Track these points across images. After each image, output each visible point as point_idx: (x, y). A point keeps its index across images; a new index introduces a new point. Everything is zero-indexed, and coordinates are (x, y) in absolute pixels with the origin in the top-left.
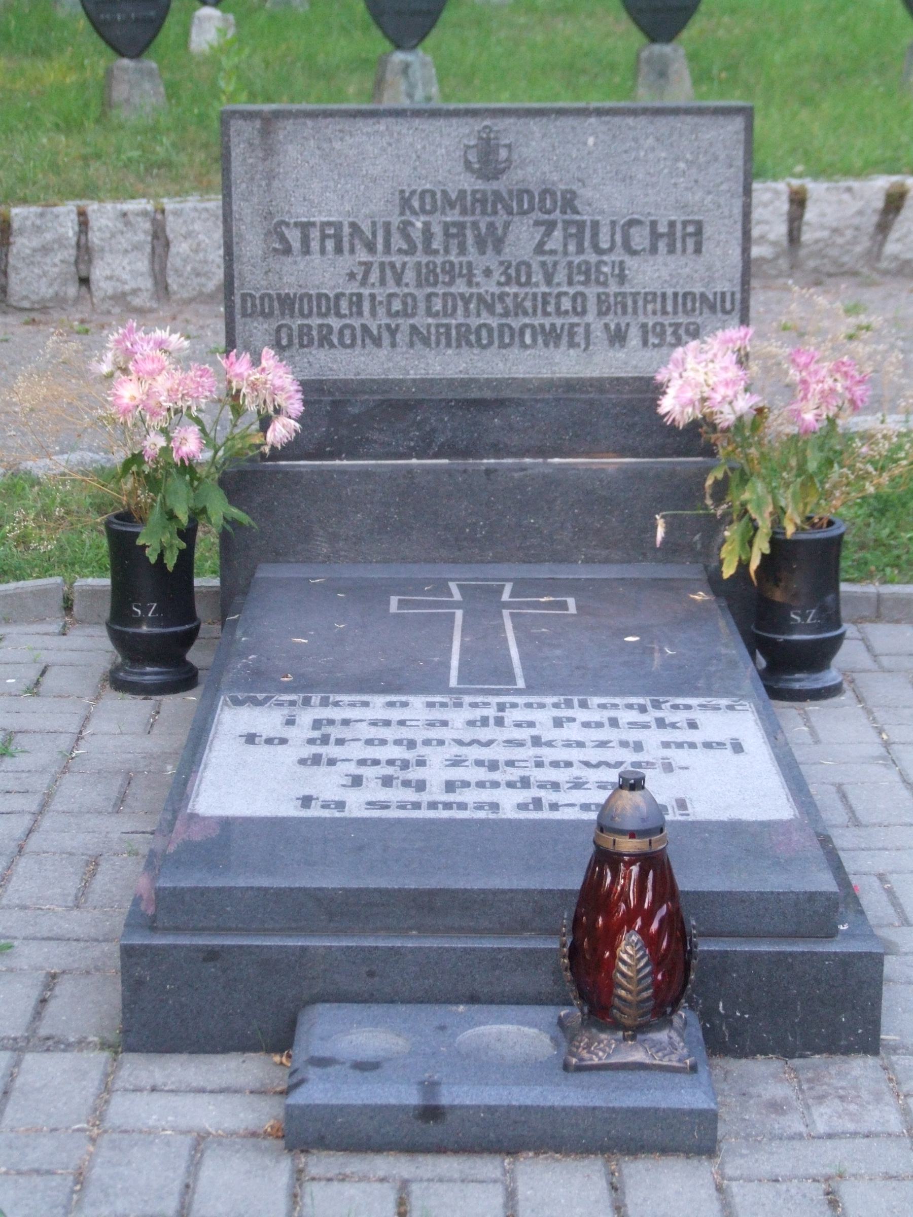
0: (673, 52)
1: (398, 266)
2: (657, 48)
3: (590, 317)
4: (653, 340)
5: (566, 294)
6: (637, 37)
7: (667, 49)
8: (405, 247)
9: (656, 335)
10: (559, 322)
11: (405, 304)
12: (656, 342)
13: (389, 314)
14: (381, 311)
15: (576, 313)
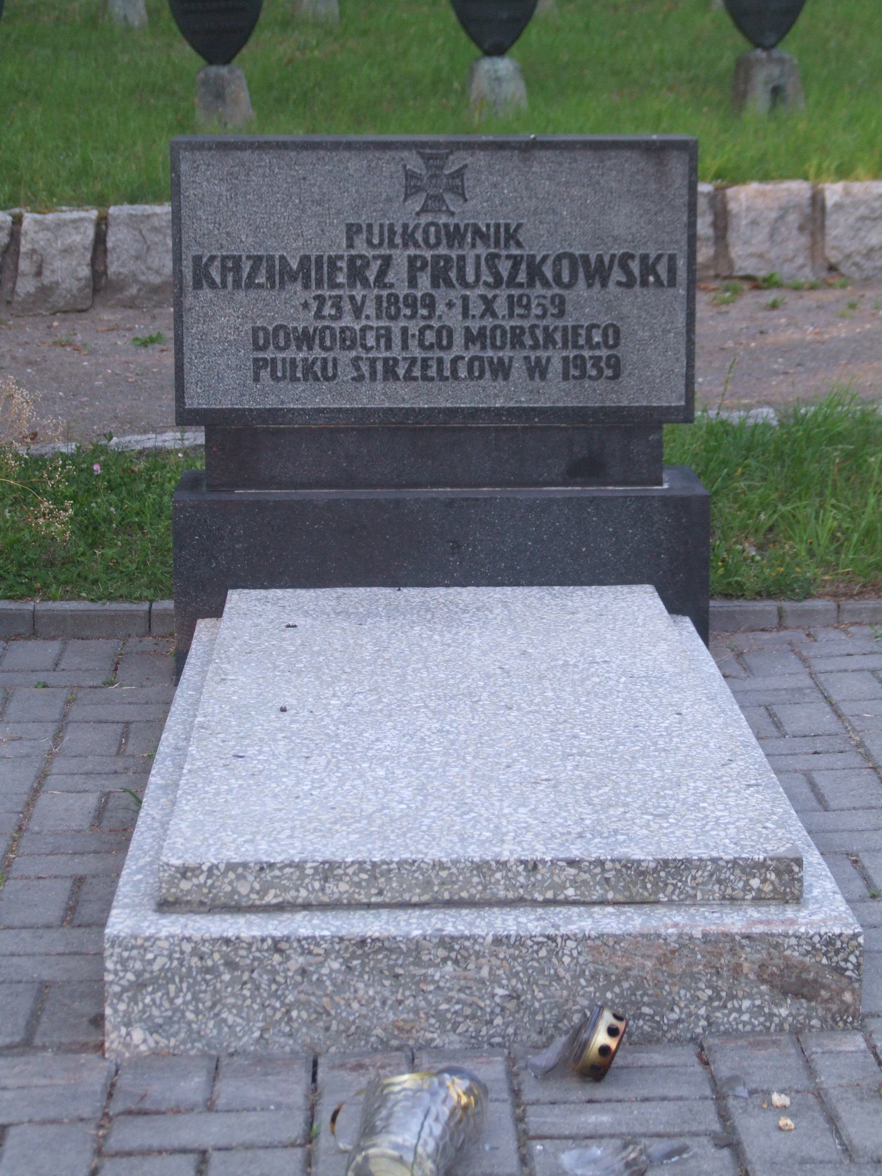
0: (237, 76)
1: (359, 299)
2: (214, 70)
3: (456, 351)
4: (574, 372)
6: (200, 61)
7: (224, 71)
8: (624, 279)
10: (587, 353)
11: (605, 335)
13: (421, 345)
14: (413, 344)
15: (441, 348)
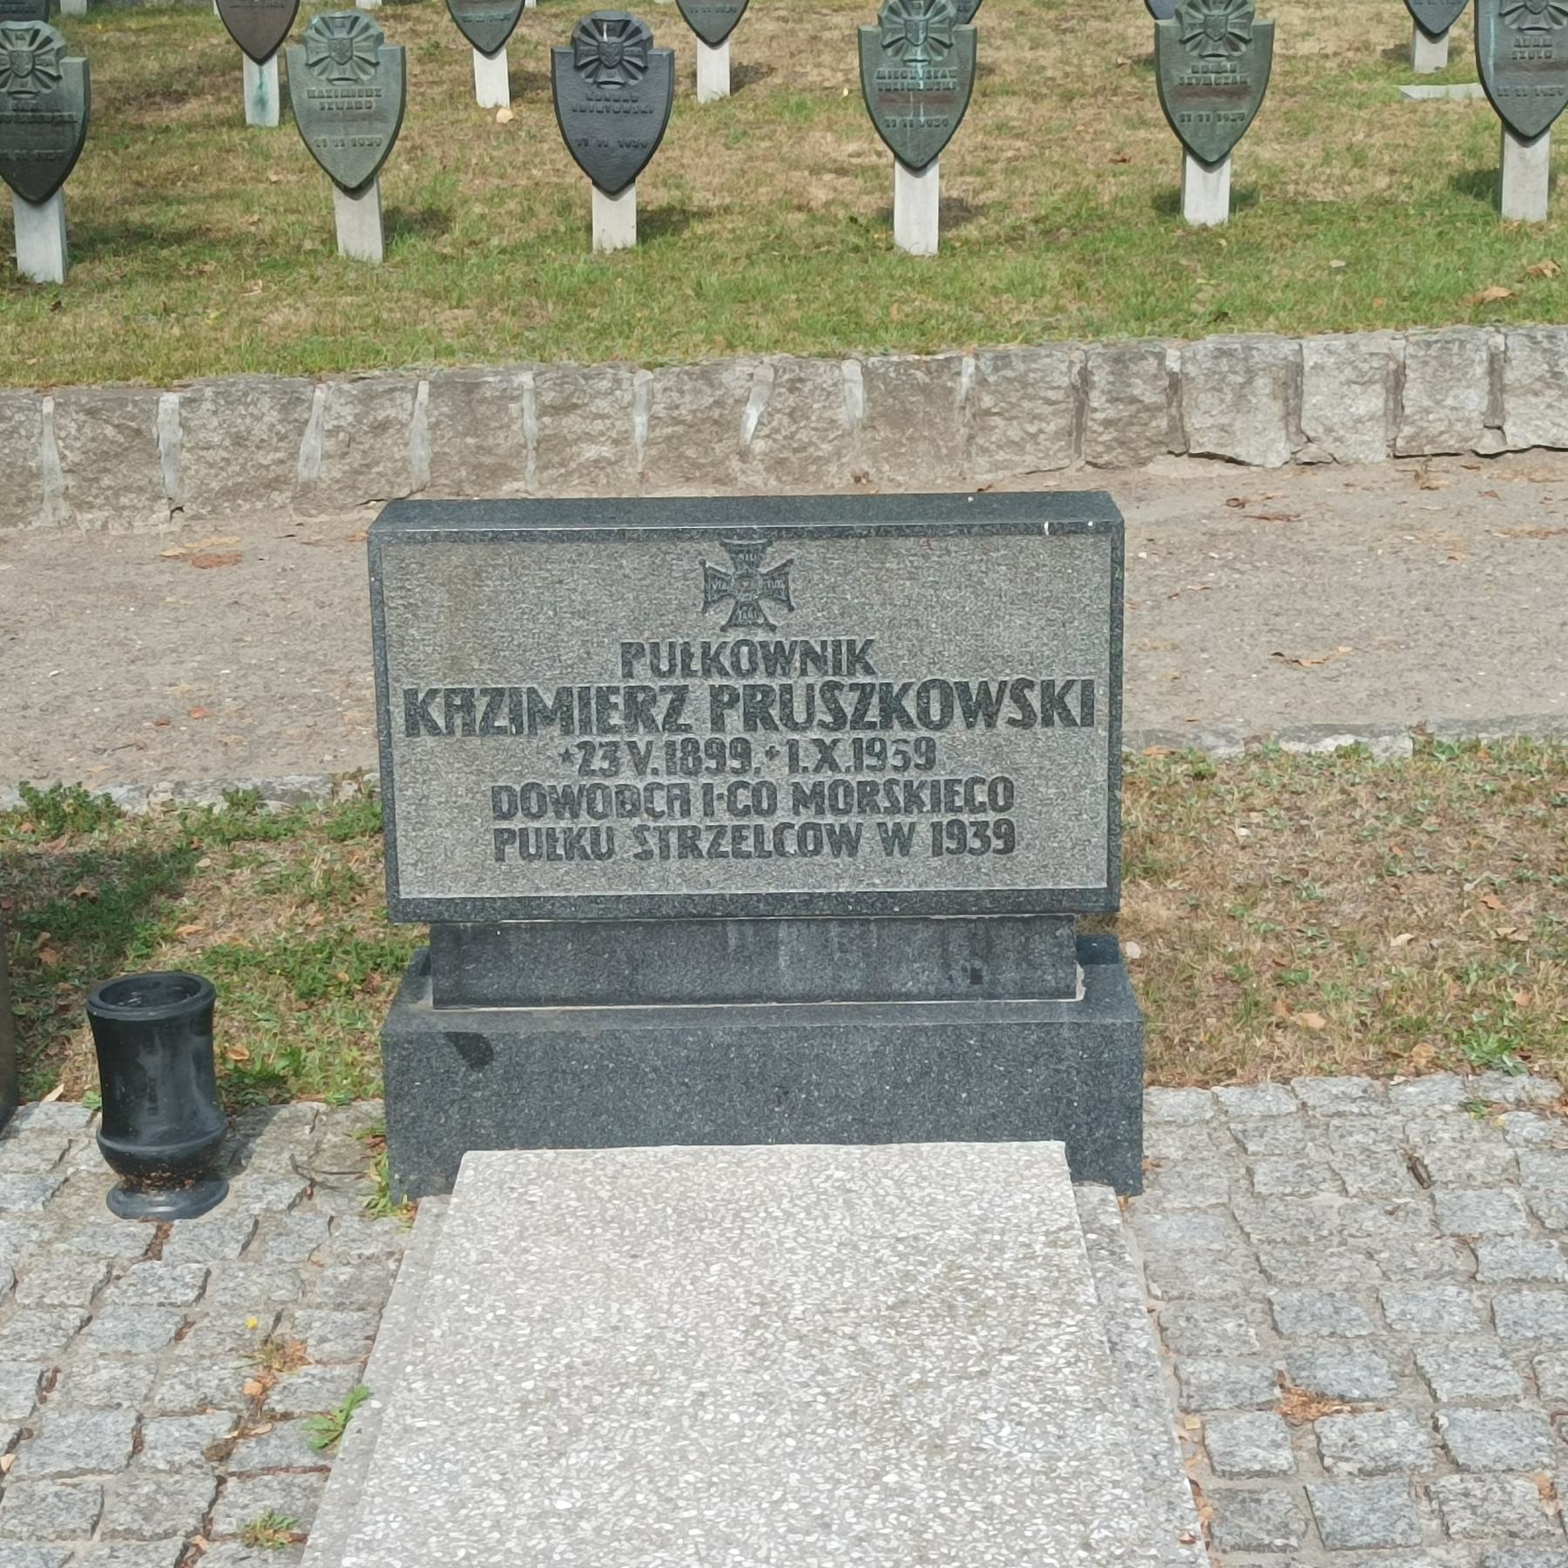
1: (642, 746)
4: (949, 844)
5: (660, 786)
8: (829, 719)
9: (951, 836)
12: (953, 846)
13: (731, 809)
14: (720, 807)
15: (760, 812)
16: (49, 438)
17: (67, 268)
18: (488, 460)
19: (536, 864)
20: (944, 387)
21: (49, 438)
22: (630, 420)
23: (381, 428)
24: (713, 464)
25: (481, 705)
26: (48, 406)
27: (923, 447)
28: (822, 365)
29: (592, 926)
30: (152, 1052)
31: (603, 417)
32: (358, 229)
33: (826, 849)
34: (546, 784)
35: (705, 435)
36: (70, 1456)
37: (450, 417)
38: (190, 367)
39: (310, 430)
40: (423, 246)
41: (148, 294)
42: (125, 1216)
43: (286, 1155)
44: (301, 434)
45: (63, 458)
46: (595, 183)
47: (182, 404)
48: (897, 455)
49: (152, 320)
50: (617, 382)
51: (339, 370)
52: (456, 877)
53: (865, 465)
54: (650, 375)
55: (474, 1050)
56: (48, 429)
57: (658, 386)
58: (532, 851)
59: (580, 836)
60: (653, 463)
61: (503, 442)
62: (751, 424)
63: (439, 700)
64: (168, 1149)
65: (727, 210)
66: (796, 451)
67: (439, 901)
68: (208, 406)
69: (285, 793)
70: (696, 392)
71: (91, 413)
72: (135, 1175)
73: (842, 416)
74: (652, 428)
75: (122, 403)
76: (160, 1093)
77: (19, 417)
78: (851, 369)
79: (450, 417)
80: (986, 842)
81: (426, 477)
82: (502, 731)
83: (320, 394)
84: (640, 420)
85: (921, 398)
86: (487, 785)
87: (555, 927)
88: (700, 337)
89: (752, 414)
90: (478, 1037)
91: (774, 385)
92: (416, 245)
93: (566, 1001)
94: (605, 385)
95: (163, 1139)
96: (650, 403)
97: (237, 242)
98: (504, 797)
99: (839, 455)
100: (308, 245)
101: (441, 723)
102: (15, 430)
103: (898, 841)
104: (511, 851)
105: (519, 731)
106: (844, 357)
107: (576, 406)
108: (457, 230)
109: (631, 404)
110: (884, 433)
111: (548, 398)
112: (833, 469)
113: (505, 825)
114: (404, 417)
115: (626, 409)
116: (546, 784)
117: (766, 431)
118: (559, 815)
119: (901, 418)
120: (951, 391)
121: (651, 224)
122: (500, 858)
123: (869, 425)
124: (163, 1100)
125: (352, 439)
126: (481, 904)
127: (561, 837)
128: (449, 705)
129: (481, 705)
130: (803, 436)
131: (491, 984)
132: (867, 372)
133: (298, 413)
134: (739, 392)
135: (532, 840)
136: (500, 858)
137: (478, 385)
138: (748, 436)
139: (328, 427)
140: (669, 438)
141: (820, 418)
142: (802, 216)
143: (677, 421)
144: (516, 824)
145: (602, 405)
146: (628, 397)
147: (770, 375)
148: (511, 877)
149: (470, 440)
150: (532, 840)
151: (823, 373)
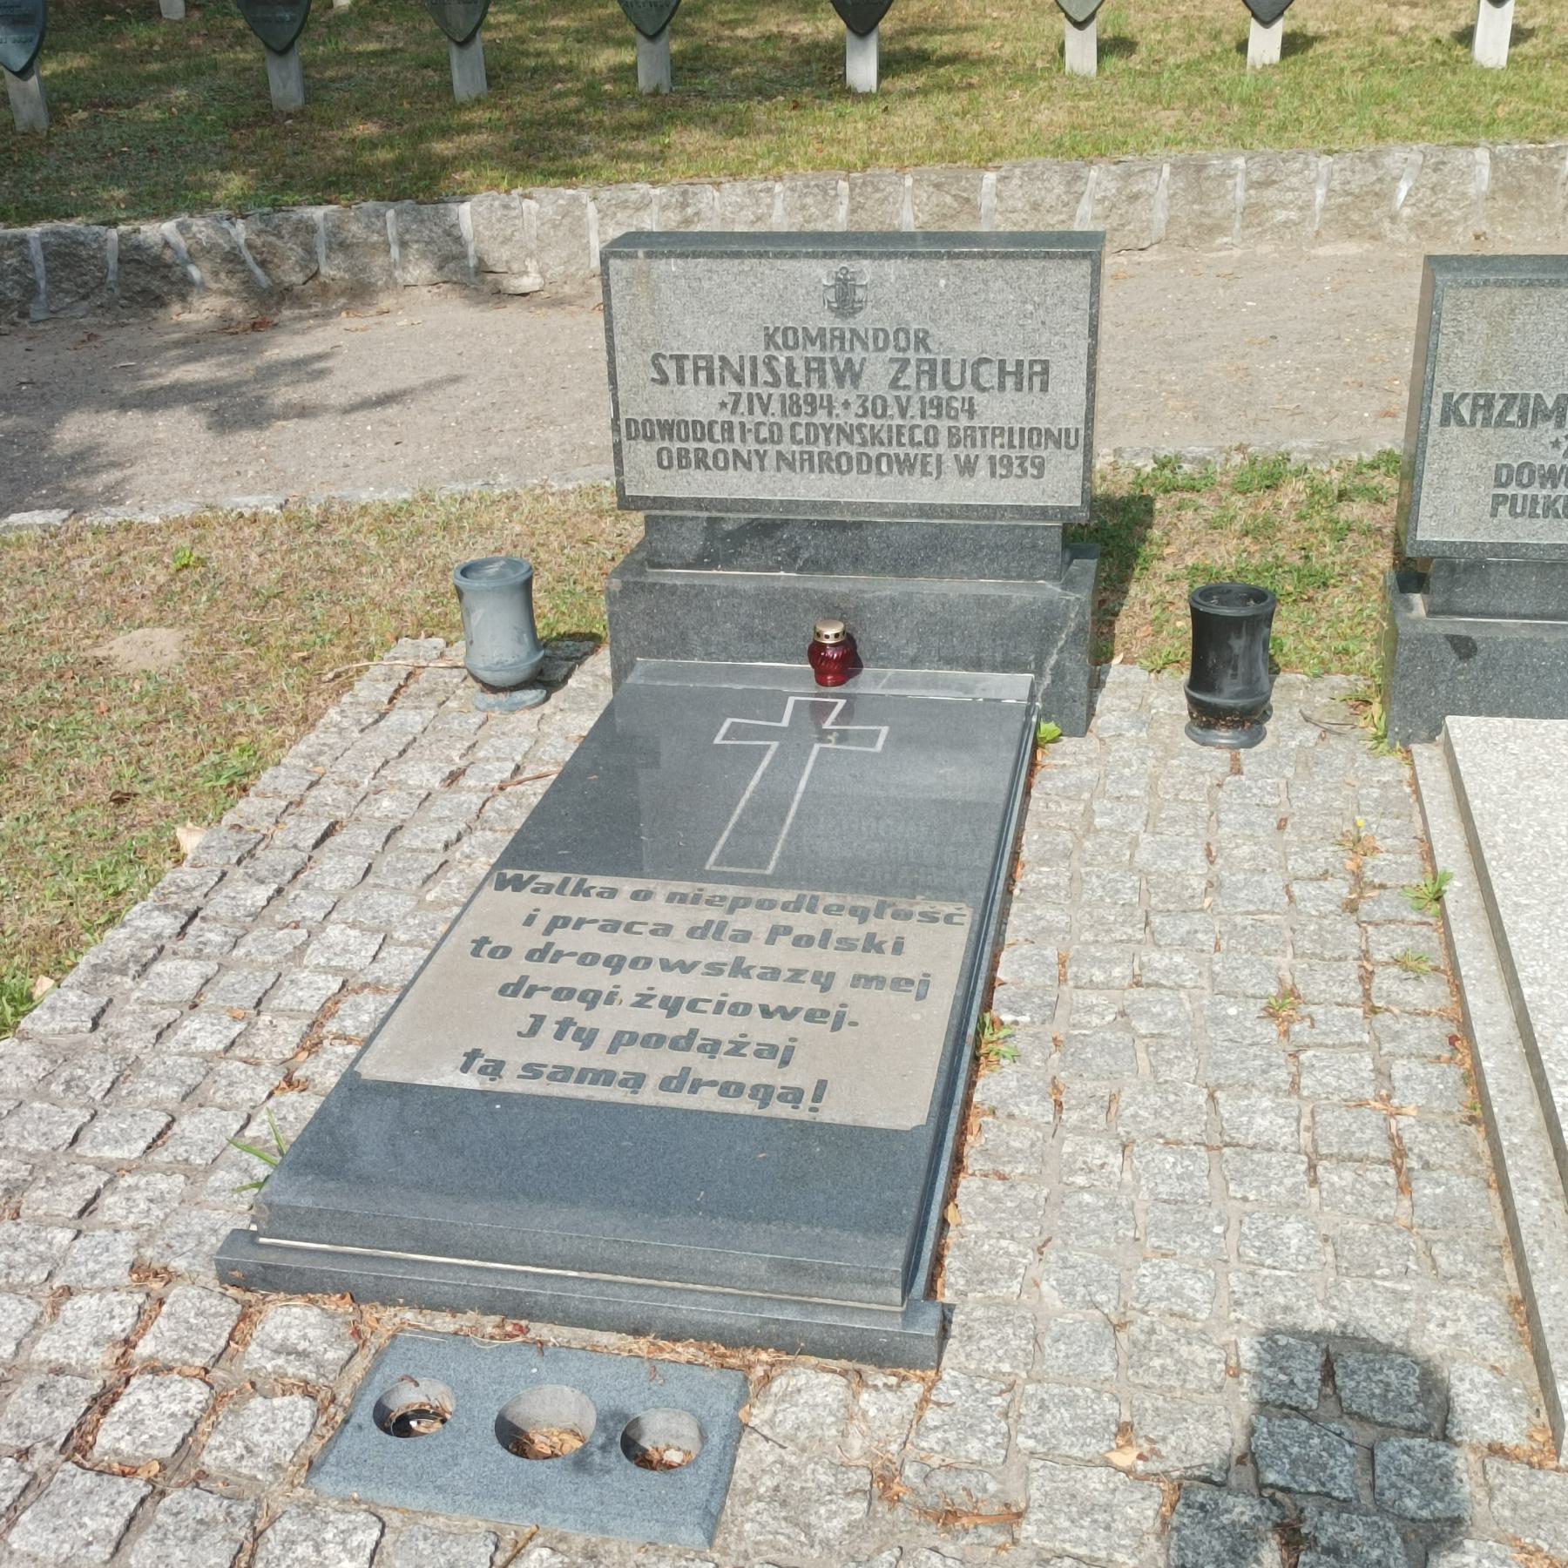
4: (1001, 471)
14: (750, 437)
16: (908, 204)
17: (879, 82)
18: (1207, 221)
19: (1520, 520)
20: (1551, 169)
21: (908, 204)
22: (1314, 192)
23: (1134, 198)
24: (1370, 225)
25: (1499, 405)
26: (909, 182)
27: (1530, 213)
28: (1460, 152)
29: (1553, 565)
30: (1239, 637)
31: (1293, 190)
32: (1081, 51)
33: (710, 454)
34: (1537, 464)
35: (1368, 204)
36: (1249, 901)
37: (1184, 190)
38: (998, 154)
39: (1084, 199)
40: (1121, 64)
41: (958, 102)
42: (1204, 744)
43: (1296, 710)
44: (1078, 202)
45: (916, 218)
46: (1254, 15)
47: (999, 181)
48: (1509, 220)
49: (957, 120)
50: (1307, 164)
51: (1102, 155)
52: (1459, 527)
53: (1484, 227)
54: (1331, 159)
55: (1464, 647)
56: (908, 198)
57: (1336, 167)
58: (1519, 510)
59: (1556, 501)
60: (1327, 223)
61: (1219, 209)
62: (1402, 195)
63: (1469, 401)
64: (1241, 702)
65: (1338, 34)
66: (1433, 216)
67: (1444, 543)
68: (1016, 181)
69: (1194, 459)
70: (1364, 171)
71: (938, 186)
72: (1206, 717)
73: (1471, 190)
74: (1328, 198)
75: (958, 179)
76: (1240, 664)
77: (890, 189)
78: (1482, 155)
79: (1184, 190)
80: (1025, 471)
81: (1163, 234)
82: (1511, 424)
83: (1093, 173)
84: (1320, 192)
85: (1533, 177)
86: (1492, 463)
87: (1526, 565)
88: (1354, 130)
89: (1403, 188)
90: (1469, 639)
91: (1422, 167)
92: (1115, 63)
93: (1525, 617)
94: (1297, 166)
95: (1238, 695)
96: (1330, 180)
97: (991, 61)
98: (1505, 472)
99: (1466, 219)
100: (1039, 64)
101: (1467, 418)
102: (886, 198)
103: (968, 468)
104: (1503, 510)
105: (1524, 425)
106: (1475, 146)
107: (1274, 182)
108: (1143, 51)
109: (1315, 181)
110: (1502, 202)
111: (1256, 176)
112: (1460, 229)
113: (1501, 491)
114: (1151, 190)
115: (1311, 185)
116: (1537, 464)
117: (1413, 201)
118: (1543, 486)
119: (1515, 191)
120: (1556, 171)
121: (1293, 44)
122: (1494, 515)
123: (1491, 197)
124: (1241, 670)
125: (1114, 206)
126: (1473, 547)
127: (1541, 501)
128: (1475, 405)
129: (1499, 405)
130: (1440, 205)
131: (1470, 603)
132: (1494, 157)
133: (1078, 187)
134: (1396, 172)
135: (1520, 503)
136: (1494, 515)
137: (1205, 167)
138: (1398, 205)
139: (1098, 197)
140: (1340, 206)
141: (1454, 191)
142: (1394, 38)
143: (1348, 194)
144: (1509, 491)
145: (1294, 180)
146: (1313, 175)
147: (1420, 159)
148: (1499, 529)
149: (1196, 207)
150: (1520, 503)
151: (1460, 157)
